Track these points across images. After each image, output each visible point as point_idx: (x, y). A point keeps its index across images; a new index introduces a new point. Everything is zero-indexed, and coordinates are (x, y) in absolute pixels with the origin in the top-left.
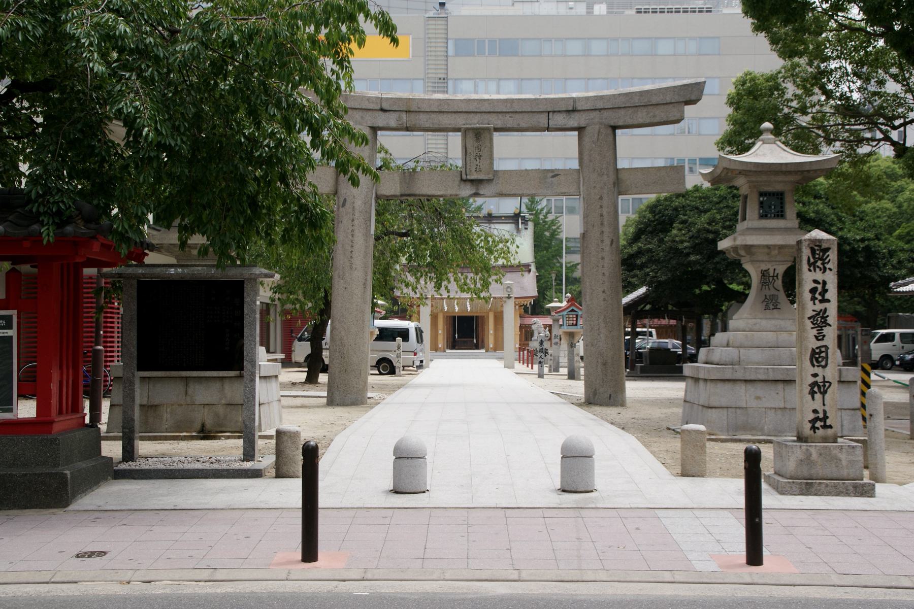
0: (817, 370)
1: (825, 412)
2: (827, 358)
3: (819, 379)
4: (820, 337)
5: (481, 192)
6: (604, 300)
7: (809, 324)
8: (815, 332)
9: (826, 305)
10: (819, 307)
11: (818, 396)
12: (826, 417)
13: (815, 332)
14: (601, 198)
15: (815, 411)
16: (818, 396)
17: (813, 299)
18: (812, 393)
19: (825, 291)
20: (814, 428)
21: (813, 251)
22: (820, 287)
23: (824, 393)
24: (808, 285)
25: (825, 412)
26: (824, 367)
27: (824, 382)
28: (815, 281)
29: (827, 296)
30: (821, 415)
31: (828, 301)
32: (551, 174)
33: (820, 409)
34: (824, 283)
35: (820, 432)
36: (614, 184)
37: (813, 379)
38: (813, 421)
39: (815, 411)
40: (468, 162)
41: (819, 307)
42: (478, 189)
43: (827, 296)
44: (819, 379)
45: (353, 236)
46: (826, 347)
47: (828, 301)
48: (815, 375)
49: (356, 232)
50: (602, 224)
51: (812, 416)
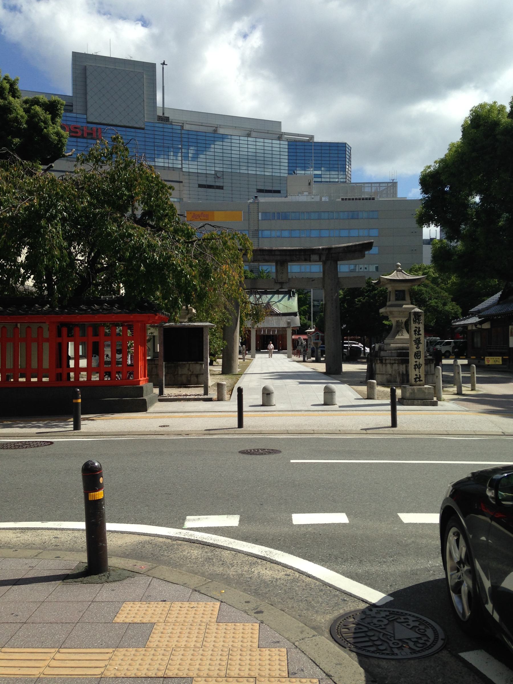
0: (417, 360)
1: (420, 375)
2: (420, 355)
3: (418, 363)
4: (418, 348)
7: (414, 343)
8: (416, 346)
9: (420, 336)
10: (417, 337)
11: (417, 369)
12: (420, 377)
13: (416, 346)
14: (332, 289)
15: (416, 375)
16: (417, 369)
17: (415, 334)
18: (415, 368)
19: (419, 331)
20: (416, 381)
21: (415, 317)
22: (418, 329)
23: (419, 368)
24: (413, 329)
25: (420, 375)
26: (419, 359)
27: (419, 364)
28: (416, 327)
29: (420, 333)
30: (418, 376)
31: (421, 334)
33: (418, 374)
34: (419, 328)
35: (418, 383)
37: (415, 363)
38: (415, 379)
39: (416, 375)
41: (417, 337)
43: (420, 333)
44: (418, 363)
46: (420, 352)
47: (421, 334)
48: (416, 362)
51: (415, 377)
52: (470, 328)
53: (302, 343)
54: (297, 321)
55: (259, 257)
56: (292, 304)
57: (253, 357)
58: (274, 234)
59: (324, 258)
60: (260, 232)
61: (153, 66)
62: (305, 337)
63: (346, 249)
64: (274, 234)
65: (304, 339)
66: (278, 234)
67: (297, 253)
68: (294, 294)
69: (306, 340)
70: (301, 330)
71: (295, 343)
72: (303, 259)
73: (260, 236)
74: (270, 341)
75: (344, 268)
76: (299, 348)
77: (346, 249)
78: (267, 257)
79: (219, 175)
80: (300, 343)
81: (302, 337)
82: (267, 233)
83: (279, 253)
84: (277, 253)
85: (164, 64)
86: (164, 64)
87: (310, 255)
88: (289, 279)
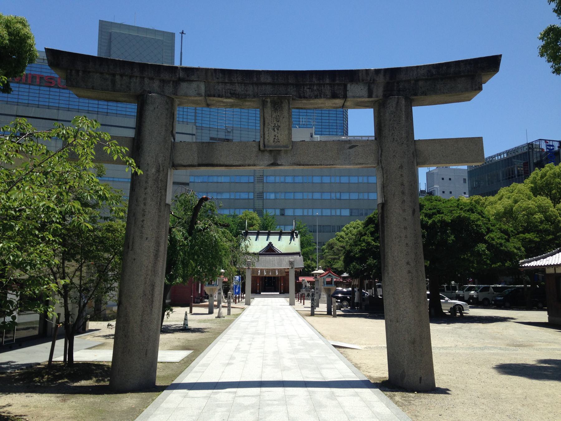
5: (279, 162)
6: (409, 272)
14: (401, 167)
32: (348, 146)
36: (413, 154)
40: (266, 133)
42: (275, 158)
45: (145, 204)
49: (149, 200)
50: (403, 193)
52: (548, 271)
53: (306, 286)
54: (300, 263)
55: (220, 87)
56: (295, 245)
57: (248, 303)
58: (278, 179)
59: (379, 92)
60: (265, 177)
61: (173, 35)
62: (311, 279)
63: (434, 71)
64: (278, 179)
65: (308, 282)
66: (282, 179)
67: (315, 80)
68: (297, 236)
69: (312, 283)
70: (306, 271)
71: (299, 287)
72: (328, 93)
73: (265, 181)
74: (270, 284)
75: (431, 121)
76: (303, 291)
77: (434, 71)
78: (239, 89)
79: (229, 130)
80: (304, 286)
81: (306, 279)
82: (271, 179)
83: (269, 80)
84: (263, 79)
85: (183, 33)
86: (183, 33)
87: (345, 86)
88: (294, 143)
